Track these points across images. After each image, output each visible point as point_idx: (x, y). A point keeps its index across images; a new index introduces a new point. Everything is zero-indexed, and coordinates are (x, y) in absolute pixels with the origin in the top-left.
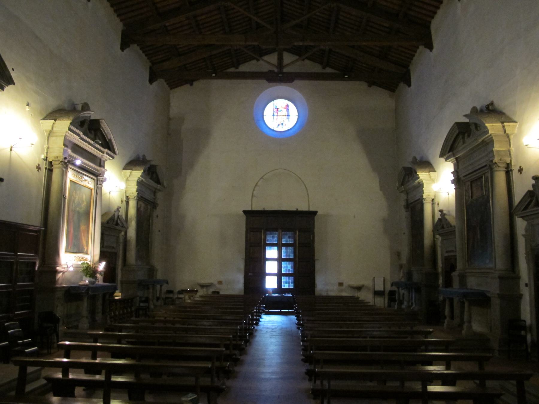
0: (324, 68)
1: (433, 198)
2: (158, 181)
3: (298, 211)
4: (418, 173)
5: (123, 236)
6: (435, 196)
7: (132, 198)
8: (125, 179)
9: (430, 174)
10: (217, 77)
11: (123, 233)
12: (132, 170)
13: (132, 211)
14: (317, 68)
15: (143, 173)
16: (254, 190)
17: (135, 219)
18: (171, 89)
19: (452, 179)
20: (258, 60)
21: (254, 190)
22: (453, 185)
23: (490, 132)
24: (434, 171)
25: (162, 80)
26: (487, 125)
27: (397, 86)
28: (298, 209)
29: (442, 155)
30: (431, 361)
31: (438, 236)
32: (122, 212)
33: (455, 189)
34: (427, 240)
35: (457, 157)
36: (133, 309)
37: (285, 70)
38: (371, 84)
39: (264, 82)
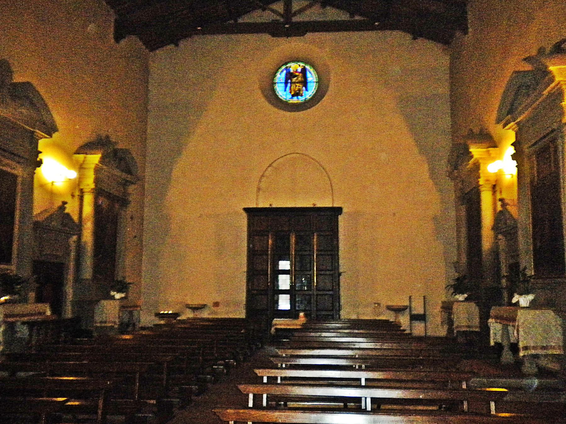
0: (352, 15)
1: (494, 184)
2: (129, 172)
3: (315, 207)
4: (471, 150)
5: (74, 242)
6: (496, 181)
7: (87, 190)
8: (77, 167)
9: (489, 151)
10: (203, 33)
11: (75, 238)
12: (86, 154)
13: (88, 209)
14: (343, 16)
15: (101, 158)
16: (260, 181)
17: (92, 219)
18: (152, 49)
19: (512, 154)
20: (264, 10)
21: (260, 181)
22: (515, 162)
23: (557, 79)
24: (495, 146)
25: (133, 37)
26: (551, 68)
27: (452, 36)
28: (315, 205)
29: (498, 121)
30: (68, 358)
31: (500, 236)
32: (71, 209)
33: (516, 166)
34: (487, 243)
35: (518, 120)
36: (478, 395)
37: (295, 19)
38: (417, 34)
39: (266, 37)
